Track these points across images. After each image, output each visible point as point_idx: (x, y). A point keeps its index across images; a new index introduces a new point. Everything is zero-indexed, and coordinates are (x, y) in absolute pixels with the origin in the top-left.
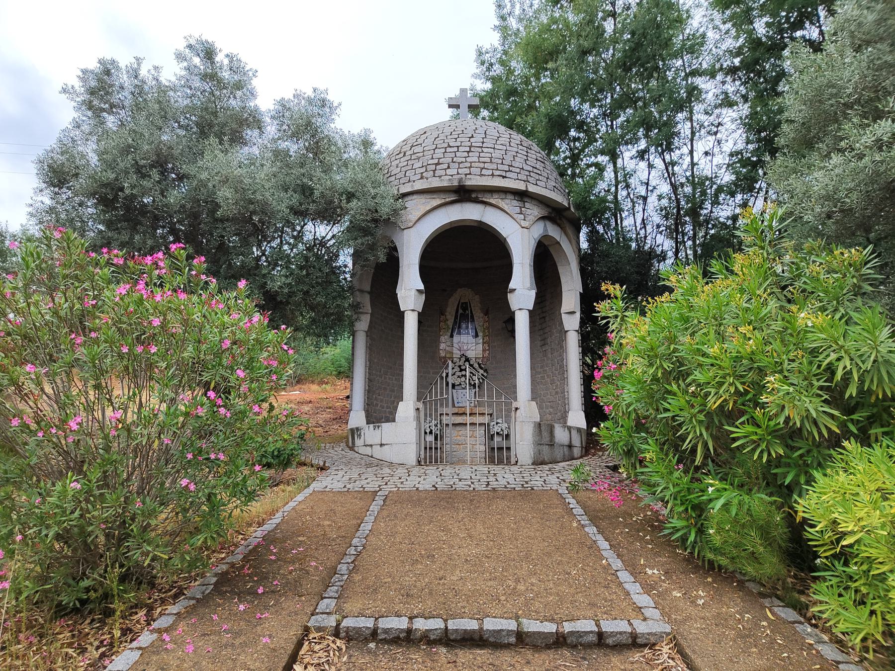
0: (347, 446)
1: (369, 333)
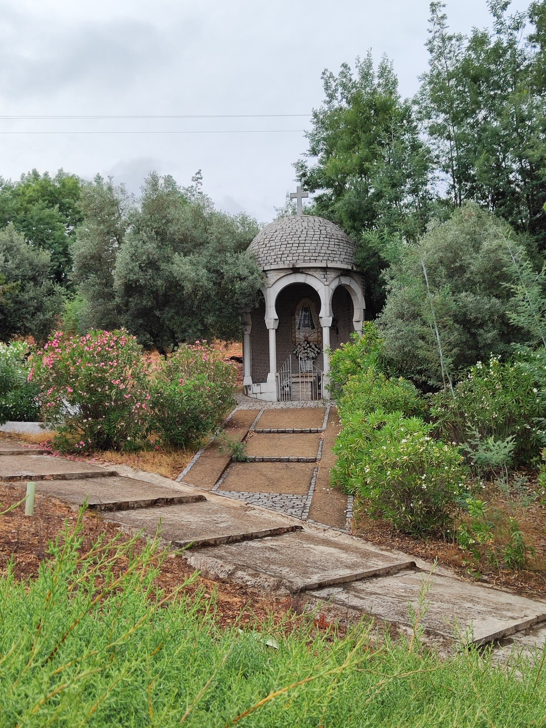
0: (244, 394)
1: (251, 335)
